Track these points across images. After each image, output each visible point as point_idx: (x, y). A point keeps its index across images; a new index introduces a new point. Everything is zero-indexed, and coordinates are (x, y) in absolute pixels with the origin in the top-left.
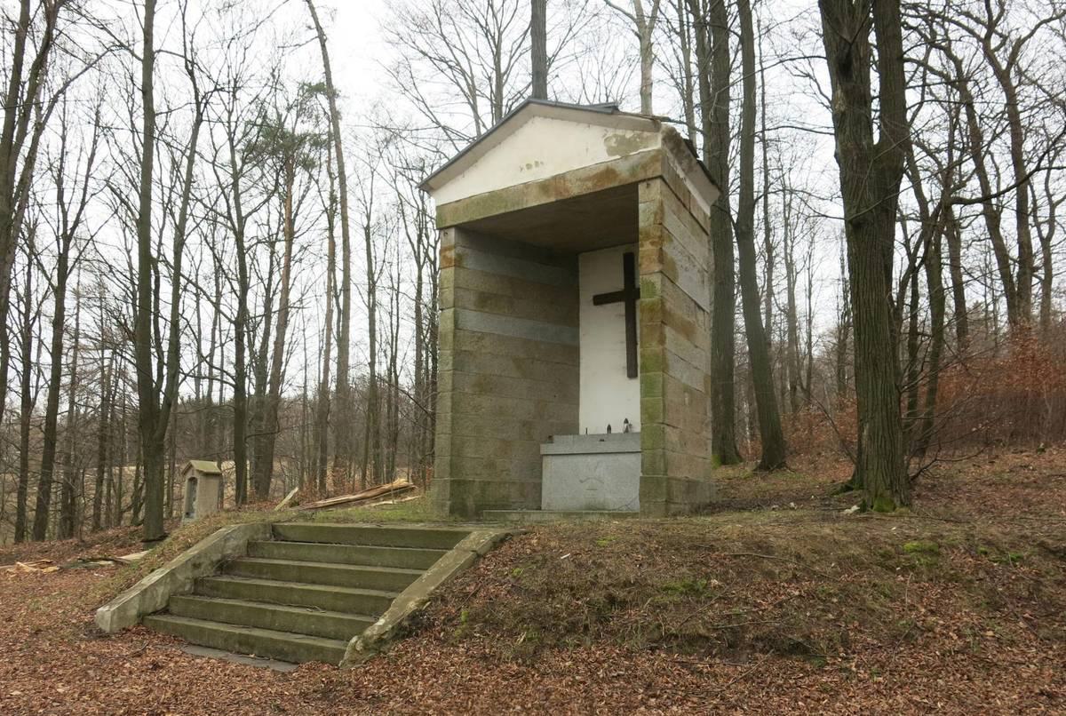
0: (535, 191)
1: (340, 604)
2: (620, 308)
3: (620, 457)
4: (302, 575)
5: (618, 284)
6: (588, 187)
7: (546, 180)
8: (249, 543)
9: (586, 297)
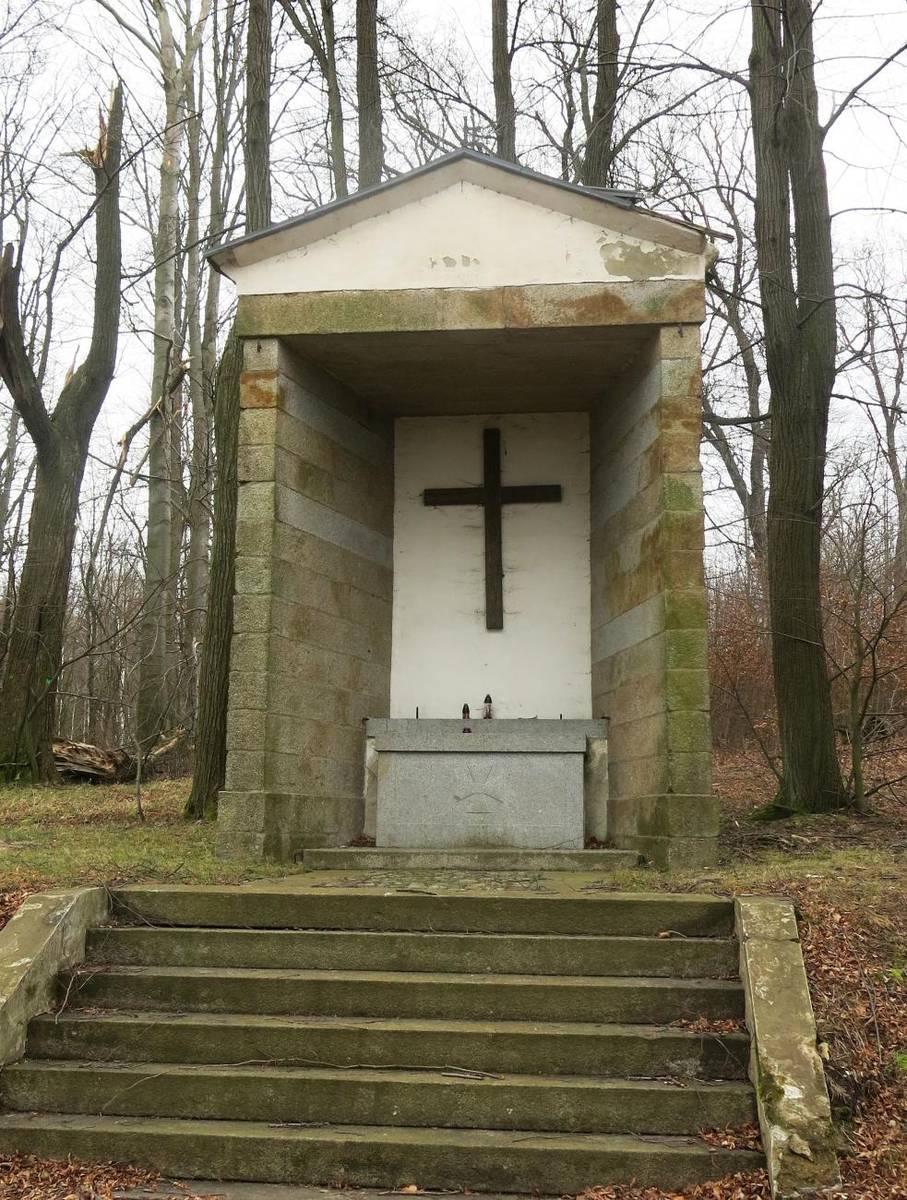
0: (460, 306)
1: (512, 1056)
3: (534, 760)
4: (242, 996)
5: (472, 475)
6: (570, 317)
7: (484, 291)
8: (89, 934)
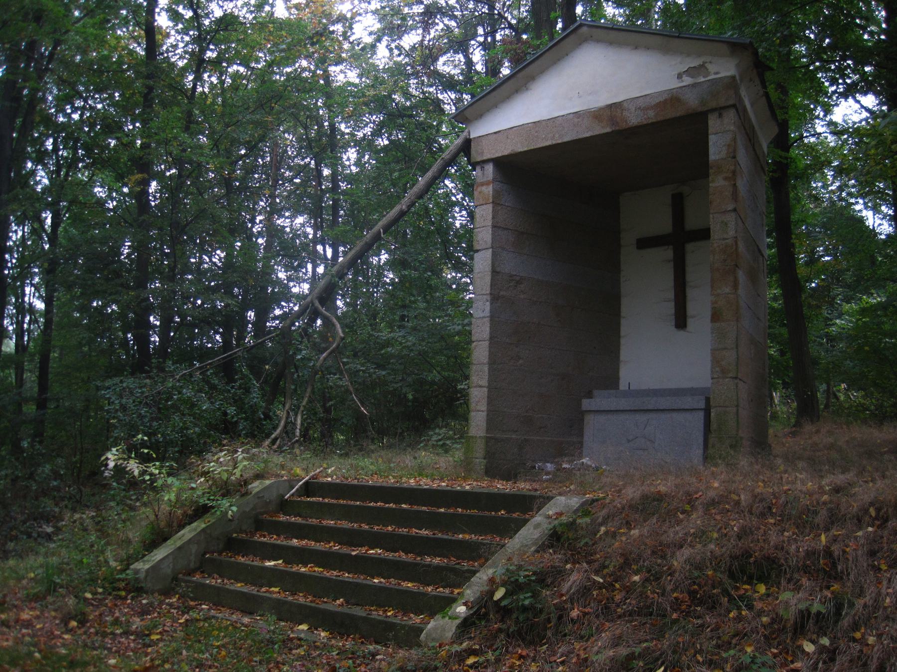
2: (668, 253)
3: (675, 415)
6: (651, 116)
9: (628, 239)
